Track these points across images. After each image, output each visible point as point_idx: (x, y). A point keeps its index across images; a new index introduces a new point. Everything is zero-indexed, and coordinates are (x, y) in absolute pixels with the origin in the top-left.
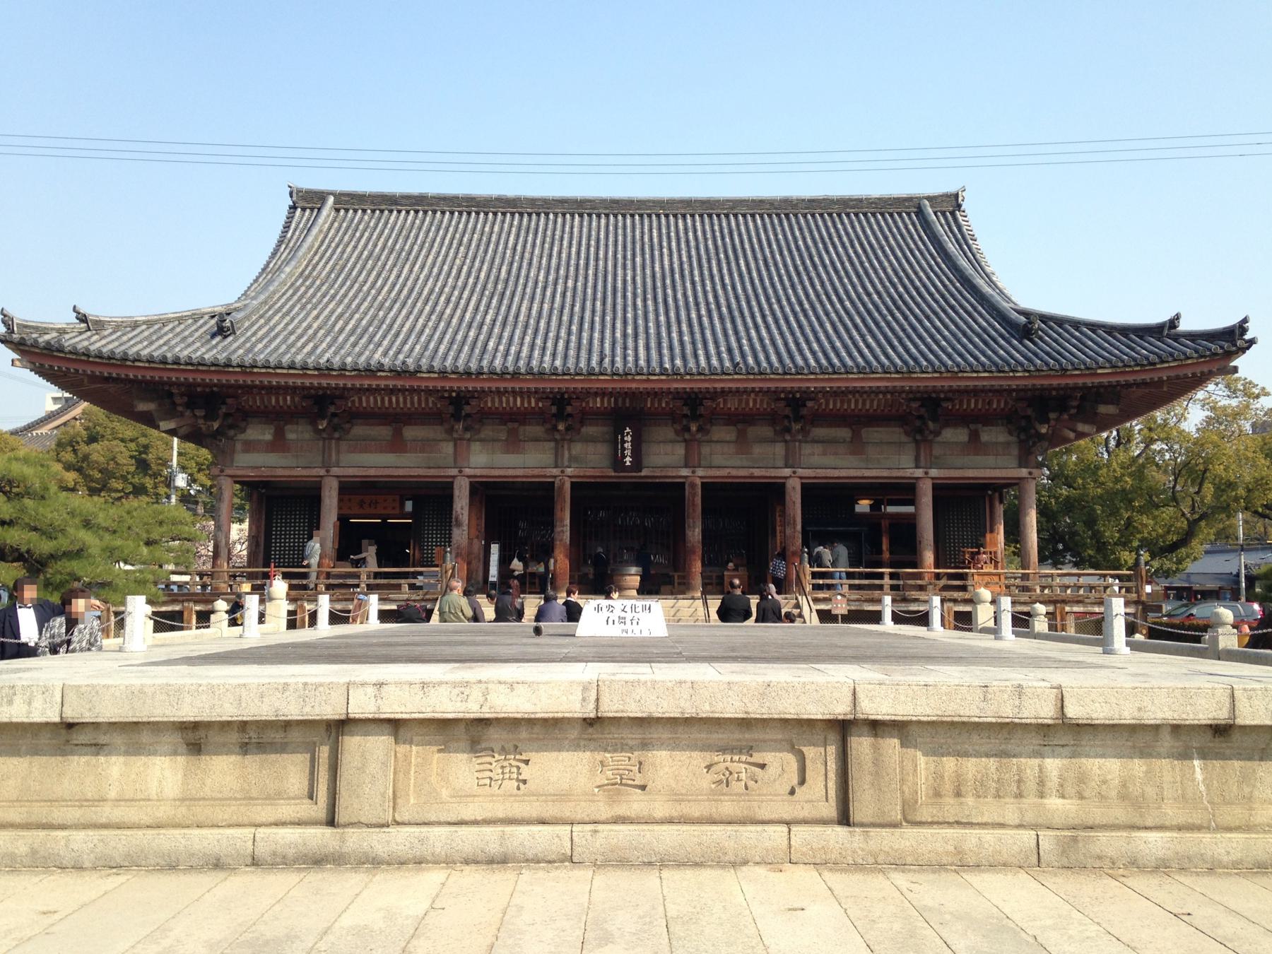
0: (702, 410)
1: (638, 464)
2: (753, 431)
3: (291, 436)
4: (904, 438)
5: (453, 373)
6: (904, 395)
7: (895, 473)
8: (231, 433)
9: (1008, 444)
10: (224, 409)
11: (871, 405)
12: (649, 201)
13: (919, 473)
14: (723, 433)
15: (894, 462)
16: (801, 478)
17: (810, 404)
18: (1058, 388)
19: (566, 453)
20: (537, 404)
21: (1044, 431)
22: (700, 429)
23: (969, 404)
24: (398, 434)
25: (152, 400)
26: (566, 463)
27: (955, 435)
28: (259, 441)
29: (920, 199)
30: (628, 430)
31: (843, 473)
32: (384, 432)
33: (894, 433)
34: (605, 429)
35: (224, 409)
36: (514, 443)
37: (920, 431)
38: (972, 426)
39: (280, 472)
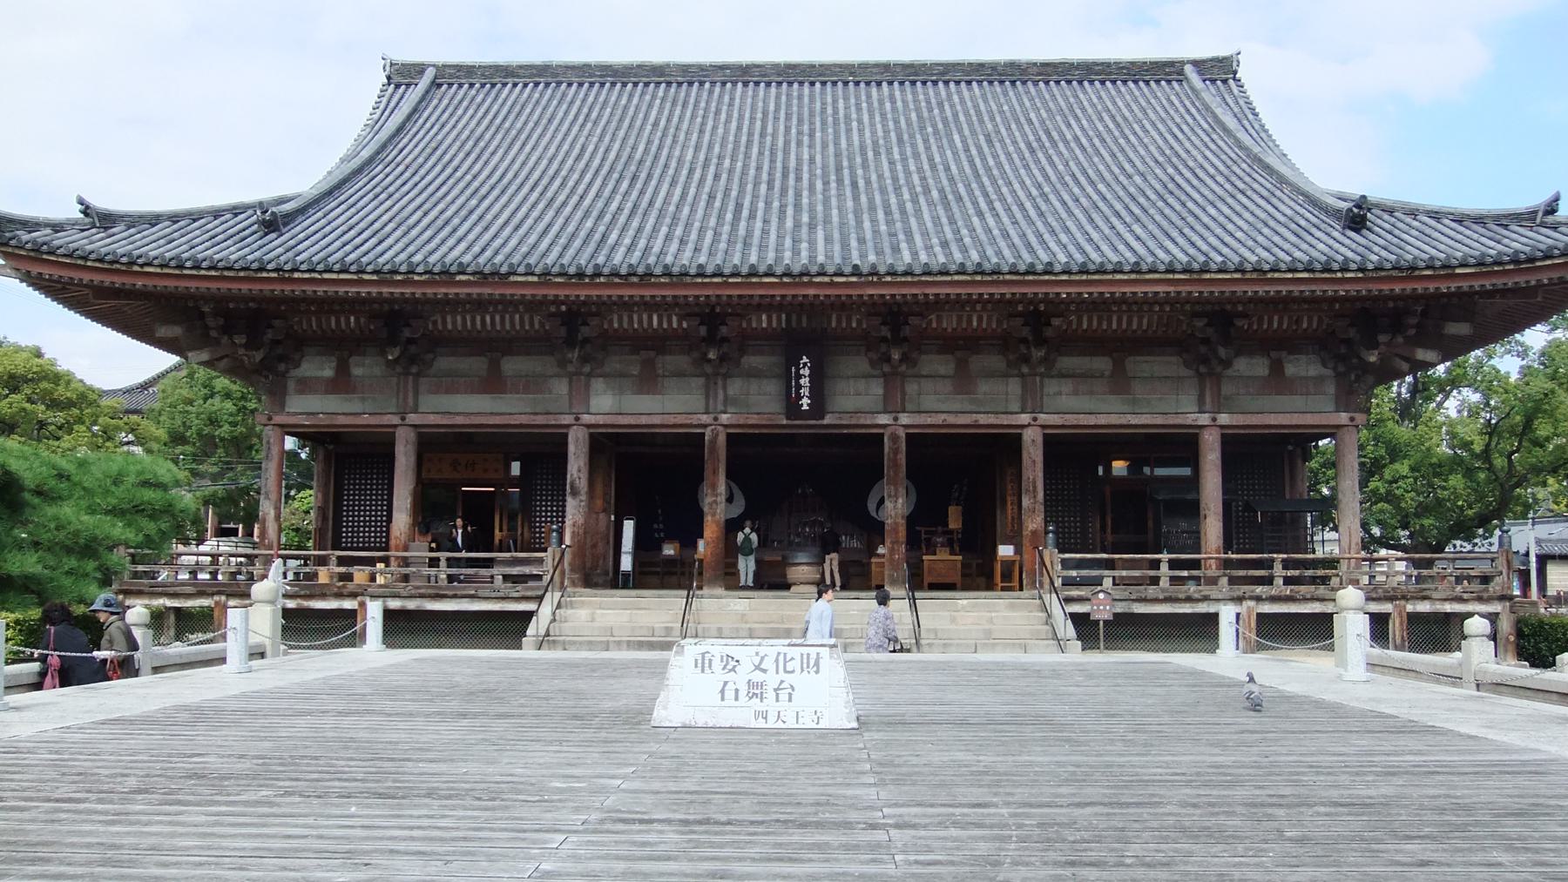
0: (906, 331)
1: (818, 408)
2: (978, 362)
3: (357, 371)
4: (1184, 372)
5: (560, 275)
6: (1188, 307)
7: (1172, 420)
8: (282, 367)
9: (1320, 380)
10: (270, 335)
11: (1139, 324)
12: (835, 65)
13: (1204, 419)
14: (940, 364)
15: (1165, 403)
16: (1043, 427)
17: (1056, 322)
18: (1393, 297)
19: (721, 392)
20: (680, 324)
21: (1373, 359)
22: (905, 358)
23: (1270, 323)
24: (495, 366)
25: (175, 323)
26: (720, 407)
27: (1252, 367)
28: (317, 378)
29: (1183, 63)
30: (805, 359)
31: (1103, 420)
32: (476, 365)
33: (1168, 365)
34: (773, 359)
35: (270, 335)
36: (648, 382)
37: (1205, 361)
38: (1273, 354)
39: (342, 420)
